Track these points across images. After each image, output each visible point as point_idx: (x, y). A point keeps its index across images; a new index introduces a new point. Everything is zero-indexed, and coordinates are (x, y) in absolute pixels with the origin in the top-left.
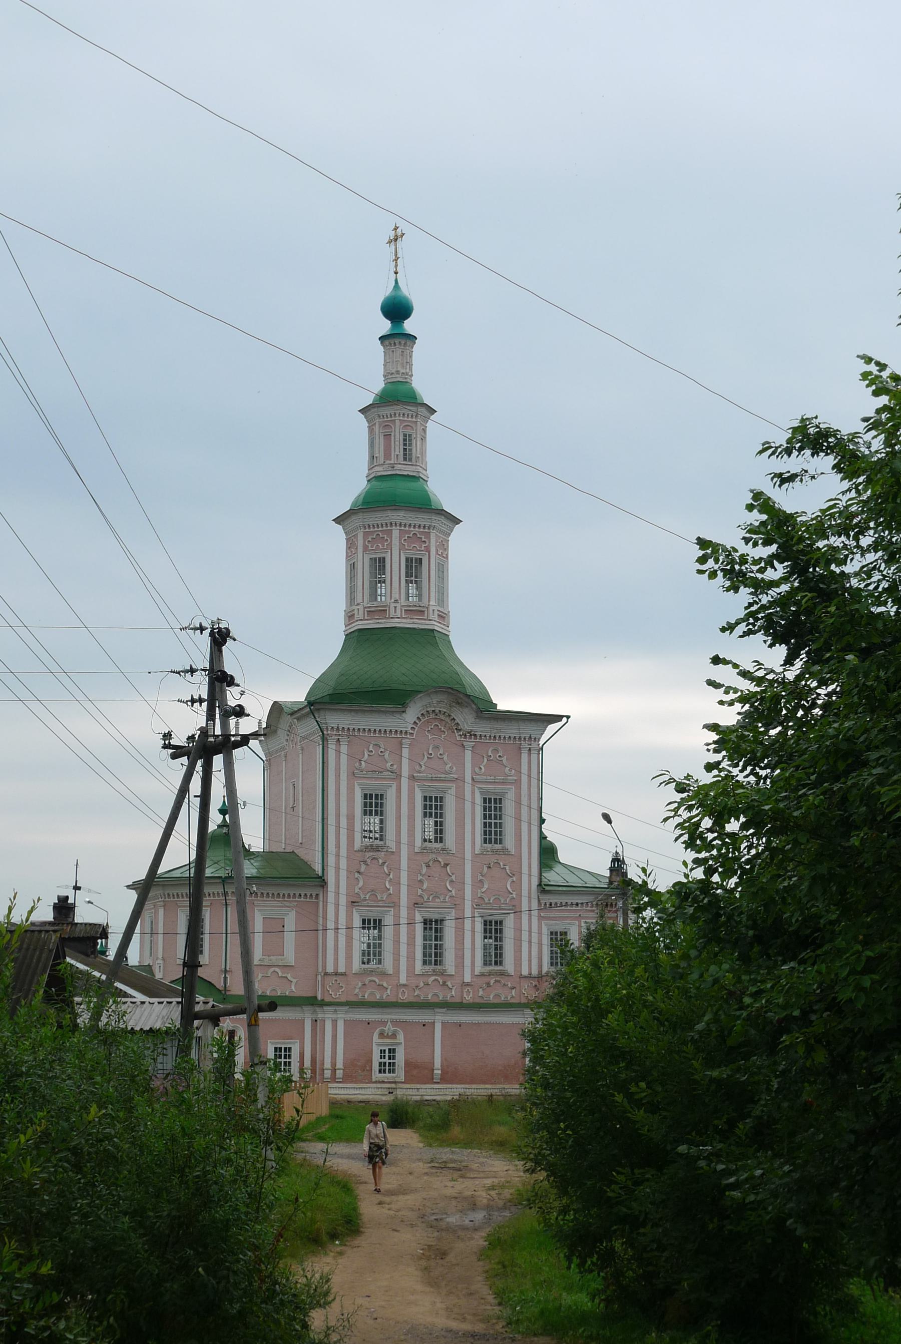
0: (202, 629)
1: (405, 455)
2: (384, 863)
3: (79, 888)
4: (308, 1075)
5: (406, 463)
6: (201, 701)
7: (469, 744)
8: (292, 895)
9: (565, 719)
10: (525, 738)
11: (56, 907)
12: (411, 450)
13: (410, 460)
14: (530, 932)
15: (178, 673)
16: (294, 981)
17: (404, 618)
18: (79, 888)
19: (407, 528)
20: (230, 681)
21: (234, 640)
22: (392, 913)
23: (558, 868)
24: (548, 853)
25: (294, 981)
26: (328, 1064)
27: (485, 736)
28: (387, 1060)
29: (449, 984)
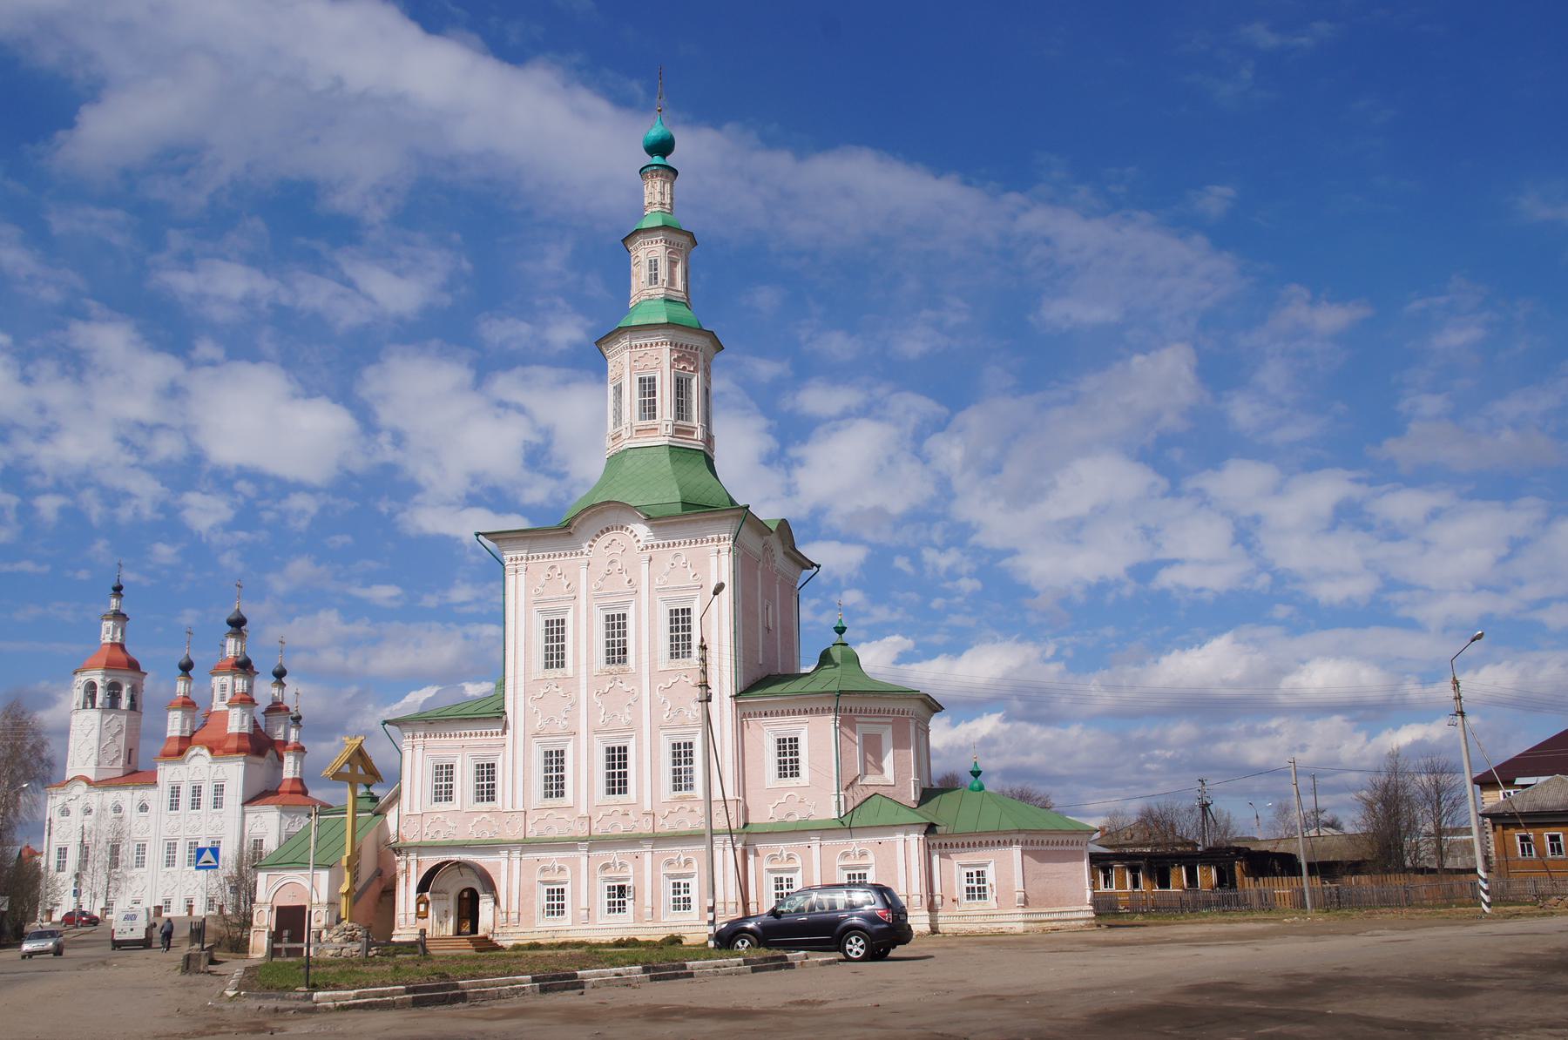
4: (514, 916)
9: (815, 569)
28: (975, 884)
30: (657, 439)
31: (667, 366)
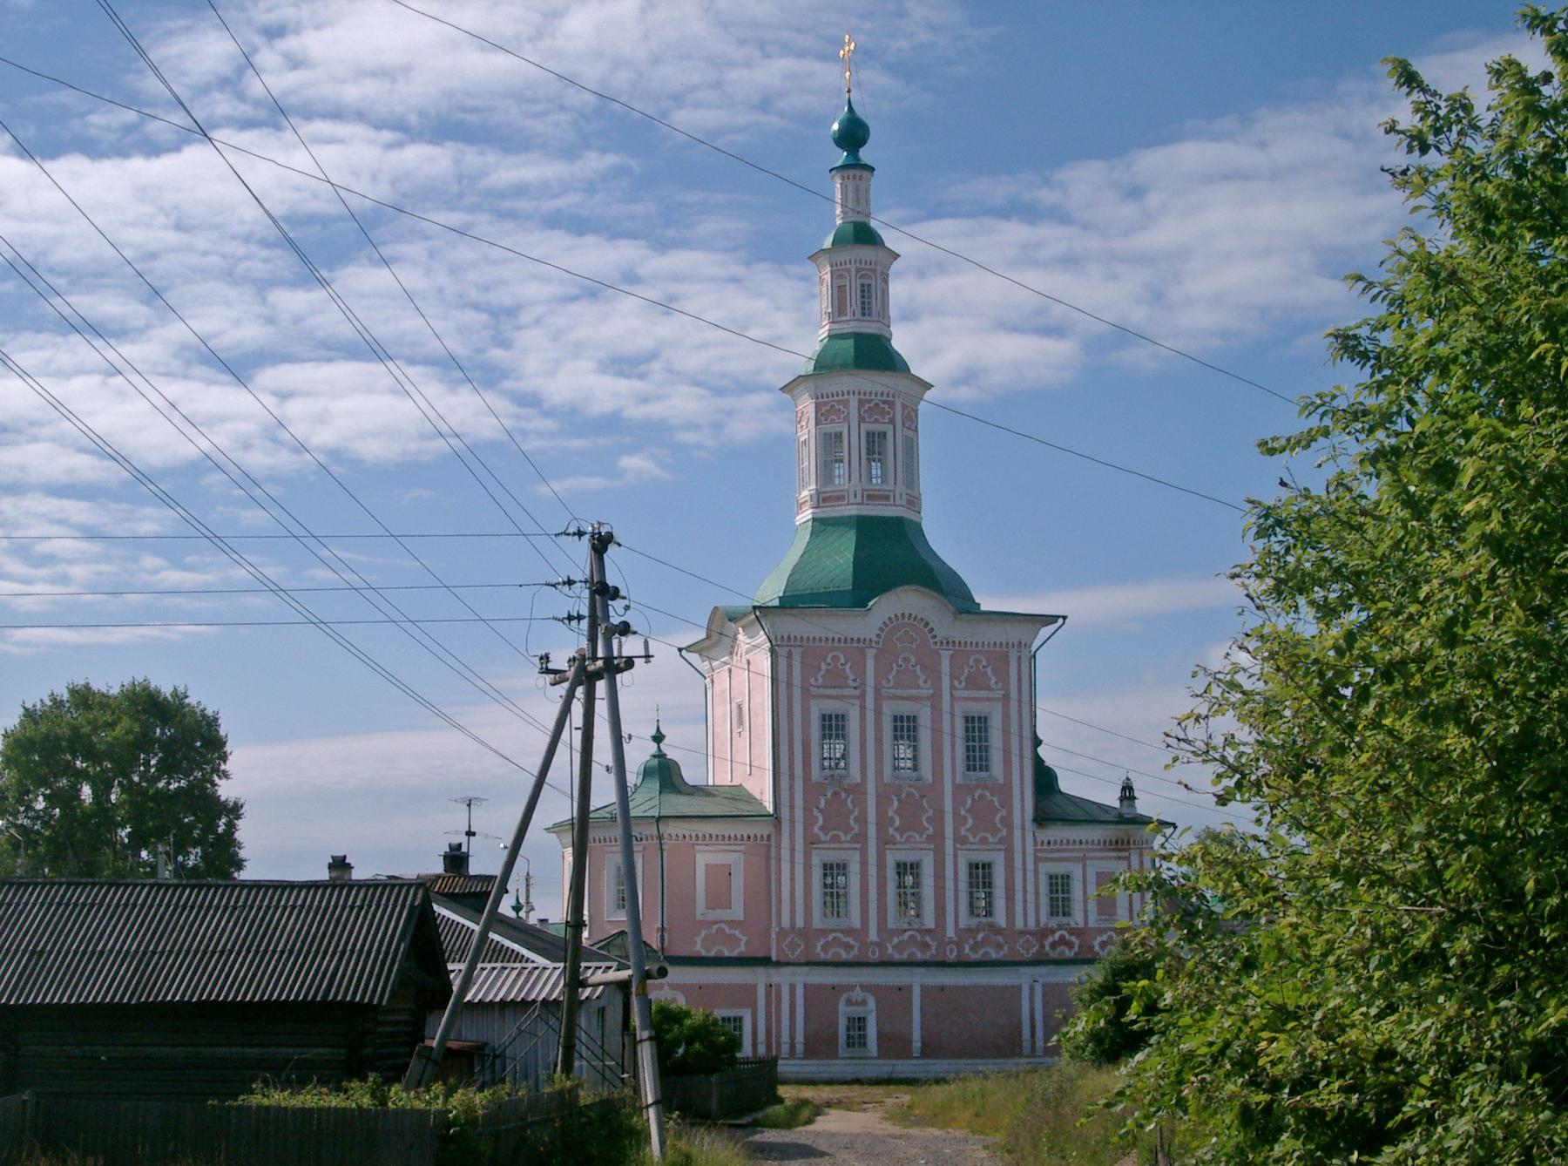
0: (580, 534)
1: (863, 309)
3: (474, 834)
6: (580, 618)
9: (1060, 621)
11: (446, 857)
12: (869, 303)
13: (870, 315)
15: (554, 586)
16: (745, 938)
18: (474, 834)
20: (615, 594)
21: (619, 545)
23: (1058, 799)
24: (1045, 779)
25: (745, 938)
26: (785, 1038)
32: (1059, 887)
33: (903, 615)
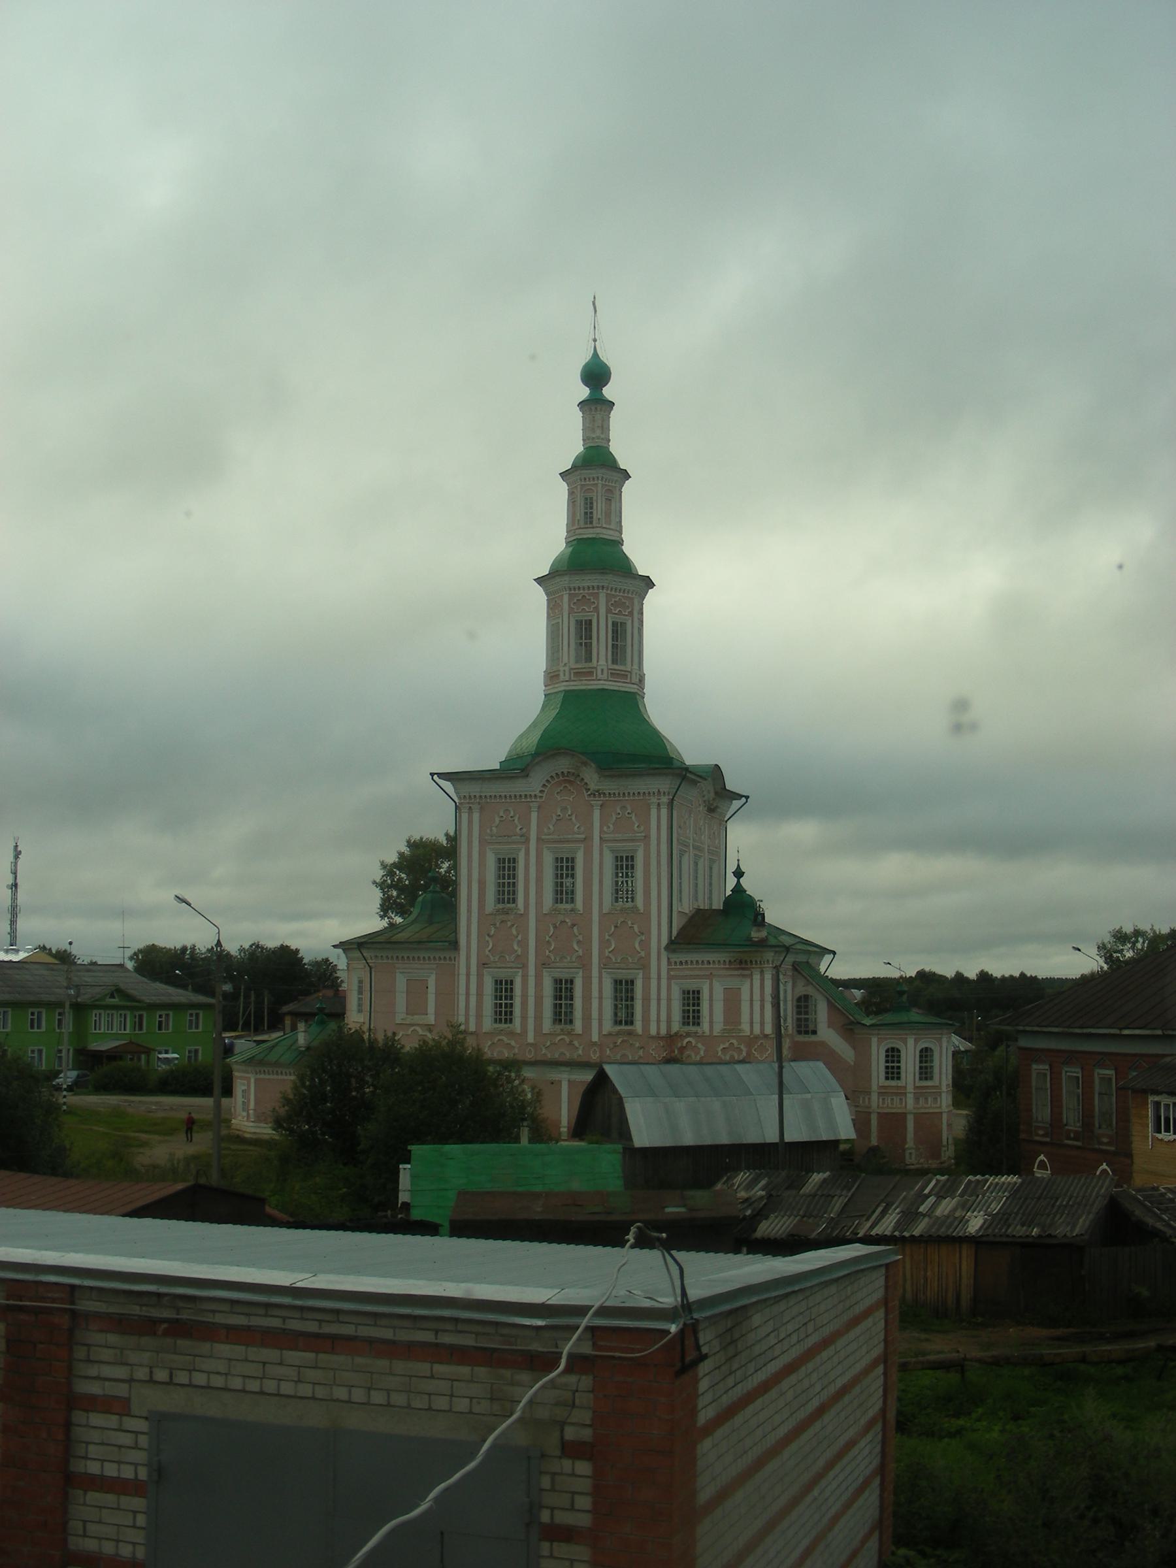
2: (513, 925)
5: (586, 526)
7: (597, 803)
8: (437, 958)
9: (744, 800)
10: (654, 793)
14: (600, 998)
17: (610, 681)
19: (577, 592)
22: (520, 974)
27: (614, 793)
29: (576, 1043)
30: (592, 682)
31: (603, 610)
32: (692, 999)
33: (552, 777)
